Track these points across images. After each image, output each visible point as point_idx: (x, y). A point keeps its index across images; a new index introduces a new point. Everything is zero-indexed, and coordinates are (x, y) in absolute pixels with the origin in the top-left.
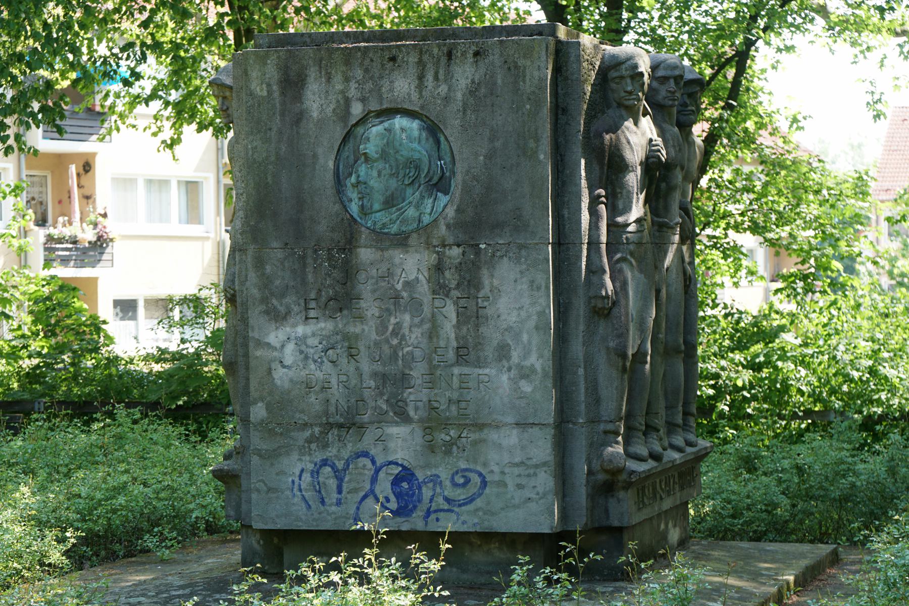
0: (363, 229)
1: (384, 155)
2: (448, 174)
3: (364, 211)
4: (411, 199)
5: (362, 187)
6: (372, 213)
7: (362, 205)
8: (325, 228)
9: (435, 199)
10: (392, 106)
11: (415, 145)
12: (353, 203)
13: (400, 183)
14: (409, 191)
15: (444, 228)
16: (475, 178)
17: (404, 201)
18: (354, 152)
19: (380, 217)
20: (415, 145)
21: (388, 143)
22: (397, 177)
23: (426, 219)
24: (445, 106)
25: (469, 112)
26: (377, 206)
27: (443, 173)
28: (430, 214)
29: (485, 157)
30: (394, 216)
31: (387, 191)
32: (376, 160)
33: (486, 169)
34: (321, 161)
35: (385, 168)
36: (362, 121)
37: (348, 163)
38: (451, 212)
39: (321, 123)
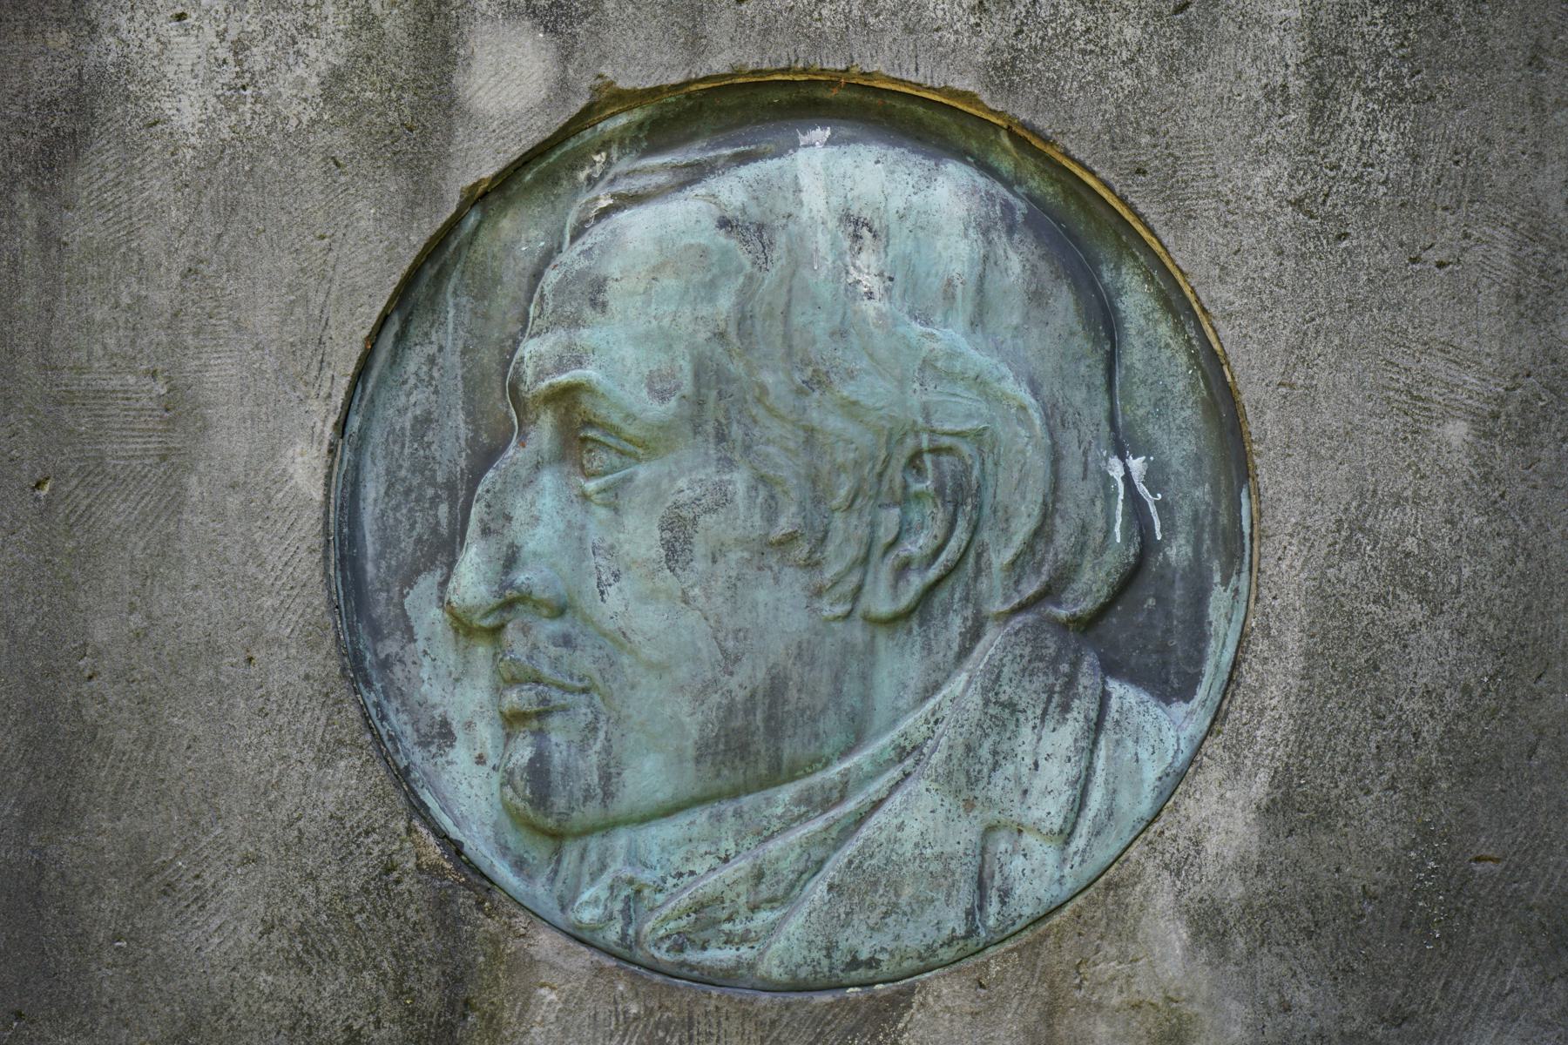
0: (546, 943)
1: (713, 405)
2: (1178, 552)
3: (547, 813)
4: (912, 723)
5: (532, 639)
6: (608, 827)
7: (539, 770)
8: (247, 935)
9: (1096, 727)
10: (777, 55)
11: (951, 336)
12: (461, 754)
13: (831, 608)
14: (898, 666)
15: (1178, 935)
16: (1404, 573)
17: (857, 737)
18: (472, 386)
19: (676, 862)
20: (951, 336)
21: (743, 319)
22: (812, 564)
23: (1035, 874)
24: (1172, 65)
25: (1353, 106)
26: (648, 776)
27: (1147, 547)
28: (1066, 835)
29: (1485, 425)
30: (784, 849)
31: (730, 660)
32: (647, 446)
33: (1493, 509)
34: (231, 440)
35: (724, 500)
36: (539, 167)
37: (422, 467)
38: (1226, 820)
39: (232, 175)
